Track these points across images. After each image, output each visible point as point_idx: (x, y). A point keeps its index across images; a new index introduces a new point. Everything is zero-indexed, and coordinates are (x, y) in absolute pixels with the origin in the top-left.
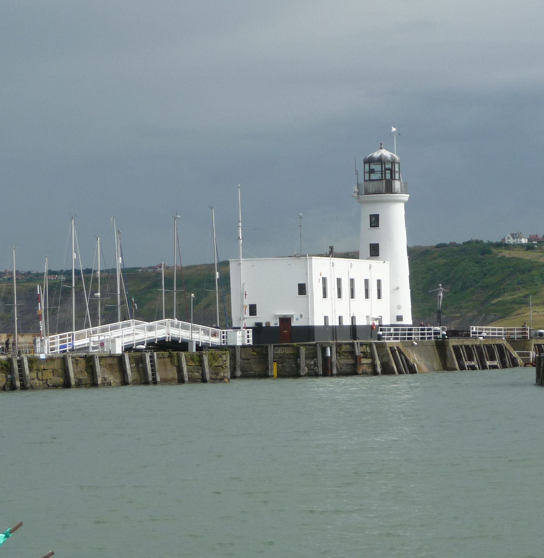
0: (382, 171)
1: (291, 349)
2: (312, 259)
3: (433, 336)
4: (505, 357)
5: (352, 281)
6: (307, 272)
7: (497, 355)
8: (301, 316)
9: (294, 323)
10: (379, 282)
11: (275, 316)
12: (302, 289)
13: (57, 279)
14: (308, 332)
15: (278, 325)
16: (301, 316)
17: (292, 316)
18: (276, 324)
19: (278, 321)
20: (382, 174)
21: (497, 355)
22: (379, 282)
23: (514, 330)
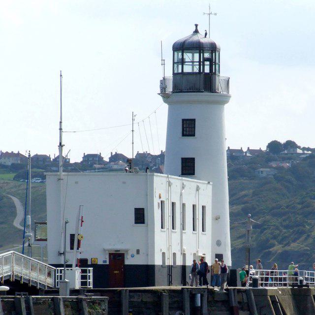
0: (200, 62)
1: (149, 295)
2: (153, 175)
3: (274, 276)
4: (266, 290)
5: (184, 205)
6: (148, 192)
7: (56, 276)
8: (138, 252)
9: (129, 261)
10: (203, 207)
11: (105, 250)
12: (140, 216)
13: (307, 285)
14: (147, 273)
15: (108, 263)
16: (138, 252)
17: (127, 251)
18: (105, 261)
19: (107, 257)
20: (200, 65)
21: (56, 276)
22: (203, 207)
23: (98, 172)
